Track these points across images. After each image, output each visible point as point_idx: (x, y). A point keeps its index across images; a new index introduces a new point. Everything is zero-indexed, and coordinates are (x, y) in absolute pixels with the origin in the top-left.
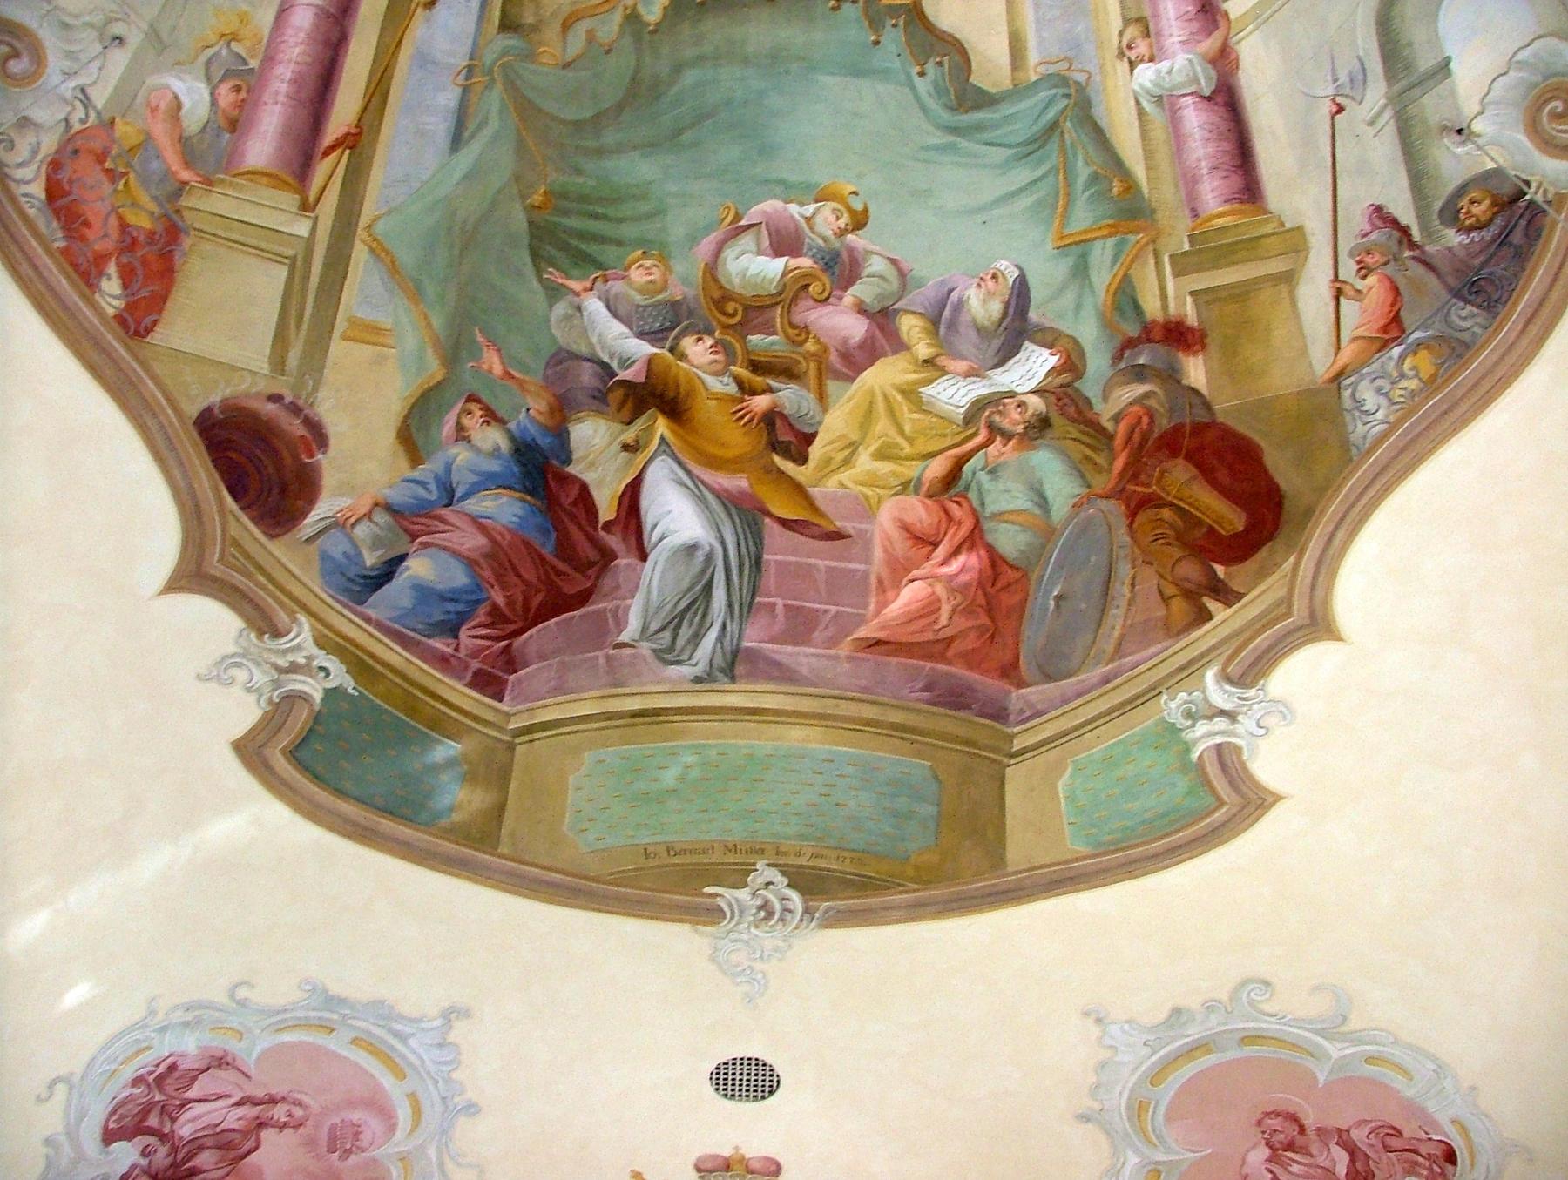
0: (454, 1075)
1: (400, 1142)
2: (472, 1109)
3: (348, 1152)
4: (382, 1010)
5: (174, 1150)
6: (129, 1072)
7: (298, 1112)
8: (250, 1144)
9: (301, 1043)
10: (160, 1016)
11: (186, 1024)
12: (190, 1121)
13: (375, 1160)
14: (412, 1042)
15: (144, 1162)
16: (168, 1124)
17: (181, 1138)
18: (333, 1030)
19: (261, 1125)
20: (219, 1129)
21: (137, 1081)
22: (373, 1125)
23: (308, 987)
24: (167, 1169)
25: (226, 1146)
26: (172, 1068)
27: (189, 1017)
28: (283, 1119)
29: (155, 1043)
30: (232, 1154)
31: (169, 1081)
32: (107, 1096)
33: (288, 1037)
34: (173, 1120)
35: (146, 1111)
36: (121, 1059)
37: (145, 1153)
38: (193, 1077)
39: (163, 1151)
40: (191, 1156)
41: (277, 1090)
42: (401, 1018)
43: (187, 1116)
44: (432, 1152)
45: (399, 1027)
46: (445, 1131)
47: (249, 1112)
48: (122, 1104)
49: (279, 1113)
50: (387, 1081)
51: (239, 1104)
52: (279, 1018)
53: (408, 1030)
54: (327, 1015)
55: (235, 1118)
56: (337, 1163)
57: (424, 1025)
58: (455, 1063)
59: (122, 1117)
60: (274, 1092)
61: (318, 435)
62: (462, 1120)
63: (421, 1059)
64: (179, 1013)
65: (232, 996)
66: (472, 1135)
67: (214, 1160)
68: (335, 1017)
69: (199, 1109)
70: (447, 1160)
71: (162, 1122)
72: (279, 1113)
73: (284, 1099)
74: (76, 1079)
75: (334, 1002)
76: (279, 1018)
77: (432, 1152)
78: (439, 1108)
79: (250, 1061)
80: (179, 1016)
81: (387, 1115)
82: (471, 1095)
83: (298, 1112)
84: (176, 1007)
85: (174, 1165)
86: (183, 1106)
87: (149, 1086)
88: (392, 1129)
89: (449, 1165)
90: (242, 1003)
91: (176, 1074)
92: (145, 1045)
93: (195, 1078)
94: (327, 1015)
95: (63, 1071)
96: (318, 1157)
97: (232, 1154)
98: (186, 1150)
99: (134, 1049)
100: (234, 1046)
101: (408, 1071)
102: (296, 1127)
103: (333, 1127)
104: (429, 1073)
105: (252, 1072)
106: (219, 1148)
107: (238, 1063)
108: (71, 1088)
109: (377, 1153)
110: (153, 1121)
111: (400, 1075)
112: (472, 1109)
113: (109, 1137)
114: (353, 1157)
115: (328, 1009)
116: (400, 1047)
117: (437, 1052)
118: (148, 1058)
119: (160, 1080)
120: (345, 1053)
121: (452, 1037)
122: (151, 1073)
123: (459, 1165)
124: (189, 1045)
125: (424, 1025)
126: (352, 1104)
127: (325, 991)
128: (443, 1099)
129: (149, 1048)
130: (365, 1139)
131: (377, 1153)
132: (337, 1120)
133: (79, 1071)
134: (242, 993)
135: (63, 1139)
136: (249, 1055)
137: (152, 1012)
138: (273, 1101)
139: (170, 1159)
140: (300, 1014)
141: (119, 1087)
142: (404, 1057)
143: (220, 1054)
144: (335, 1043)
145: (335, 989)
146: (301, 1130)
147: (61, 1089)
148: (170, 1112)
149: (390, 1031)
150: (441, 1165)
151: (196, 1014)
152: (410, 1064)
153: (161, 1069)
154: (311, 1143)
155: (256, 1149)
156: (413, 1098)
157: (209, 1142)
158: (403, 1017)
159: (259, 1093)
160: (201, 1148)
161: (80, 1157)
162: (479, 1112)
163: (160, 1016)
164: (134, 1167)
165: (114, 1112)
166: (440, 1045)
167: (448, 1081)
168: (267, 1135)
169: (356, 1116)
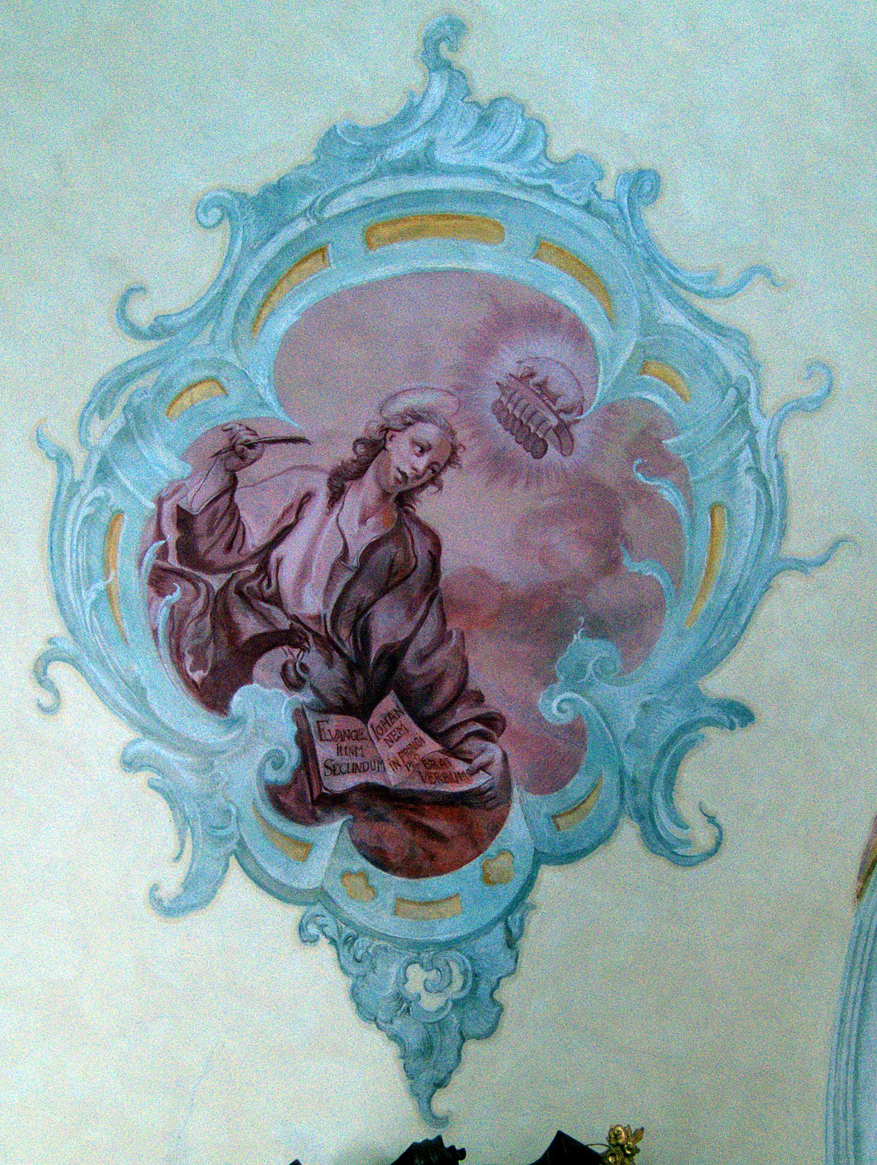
0: (559, 150)
1: (615, 345)
2: (644, 185)
3: (563, 430)
4: (346, 148)
5: (328, 645)
6: (131, 579)
7: (428, 432)
8: (421, 547)
9: (311, 314)
10: (79, 456)
11: (125, 435)
12: (303, 575)
13: (611, 408)
14: (445, 156)
15: (306, 697)
16: (276, 612)
17: (318, 618)
18: (321, 251)
19: (401, 499)
20: (354, 562)
21: (159, 580)
22: (548, 351)
23: (215, 213)
24: (351, 683)
25: (392, 580)
26: (184, 519)
27: (116, 420)
28: (422, 463)
29: (117, 501)
30: (416, 581)
31: (203, 545)
32: (141, 637)
33: (282, 322)
34: (276, 600)
35: (220, 612)
36: (96, 563)
37: (293, 682)
38: (226, 509)
39: (314, 659)
40: (362, 636)
41: (363, 421)
42: (386, 132)
43: (287, 576)
44: (672, 315)
45: (398, 152)
46: (652, 262)
47: (362, 495)
48: (176, 631)
49: (403, 457)
50: (485, 260)
51: (336, 496)
52: (232, 305)
53: (417, 143)
54: (286, 235)
55: (355, 521)
56: (567, 462)
57: (427, 110)
58: (535, 129)
59: (198, 653)
60: (359, 431)
61: (251, 683)
62: (655, 219)
63: (483, 172)
64: (97, 426)
65: (136, 333)
66: (688, 223)
67: (400, 615)
68: (302, 226)
69: (291, 553)
70: (700, 303)
71: (264, 617)
72: (403, 457)
73: (385, 429)
74: (67, 644)
75: (271, 203)
76: (232, 305)
77: (672, 315)
78: (599, 230)
79: (275, 416)
80: (102, 431)
81: (547, 317)
82: (615, 163)
83: (428, 432)
84: (83, 423)
85: (355, 667)
86: (264, 568)
87: (180, 574)
88: (577, 333)
89: (716, 310)
90: (159, 329)
91: (201, 526)
92: (105, 517)
93: (233, 511)
94: (286, 235)
95: (39, 647)
96: (533, 478)
97: (416, 581)
98: (344, 633)
99: (98, 541)
100: (229, 408)
101: (495, 212)
102: (452, 460)
103: (498, 408)
104: (522, 186)
105: (297, 428)
106: (384, 591)
107: (265, 432)
108: (73, 661)
109: (602, 391)
110: (249, 626)
111: (487, 231)
112: (644, 185)
113: (214, 695)
114: (576, 430)
115: (275, 221)
116: (437, 183)
117: (491, 137)
118: (133, 531)
119: (187, 550)
120: (380, 272)
121: (484, 92)
122: (163, 553)
123: (728, 295)
124: (166, 464)
125: (427, 110)
126: (482, 349)
127: (241, 197)
128: (587, 207)
129: (118, 515)
130: (559, 381)
131: (602, 391)
132: (492, 395)
133: (57, 627)
134: (142, 313)
135: (147, 745)
136: (263, 405)
137: (61, 459)
138: (374, 447)
139: (339, 665)
140: (253, 270)
141: (141, 617)
142: (461, 195)
143: (222, 442)
144: (352, 270)
145: (253, 180)
146: (465, 458)
147: (59, 672)
148: (257, 583)
149: (399, 169)
150: (702, 319)
151: (126, 405)
152: (480, 198)
153: (172, 535)
154: (498, 466)
155: (437, 544)
156: (543, 248)
157: (363, 592)
158: (383, 130)
159: (343, 452)
160: (363, 612)
161: (207, 757)
162: (657, 178)
163: (79, 456)
164: (299, 715)
165: (177, 656)
166: (485, 120)
167: (560, 170)
168: (428, 507)
169: (508, 361)
